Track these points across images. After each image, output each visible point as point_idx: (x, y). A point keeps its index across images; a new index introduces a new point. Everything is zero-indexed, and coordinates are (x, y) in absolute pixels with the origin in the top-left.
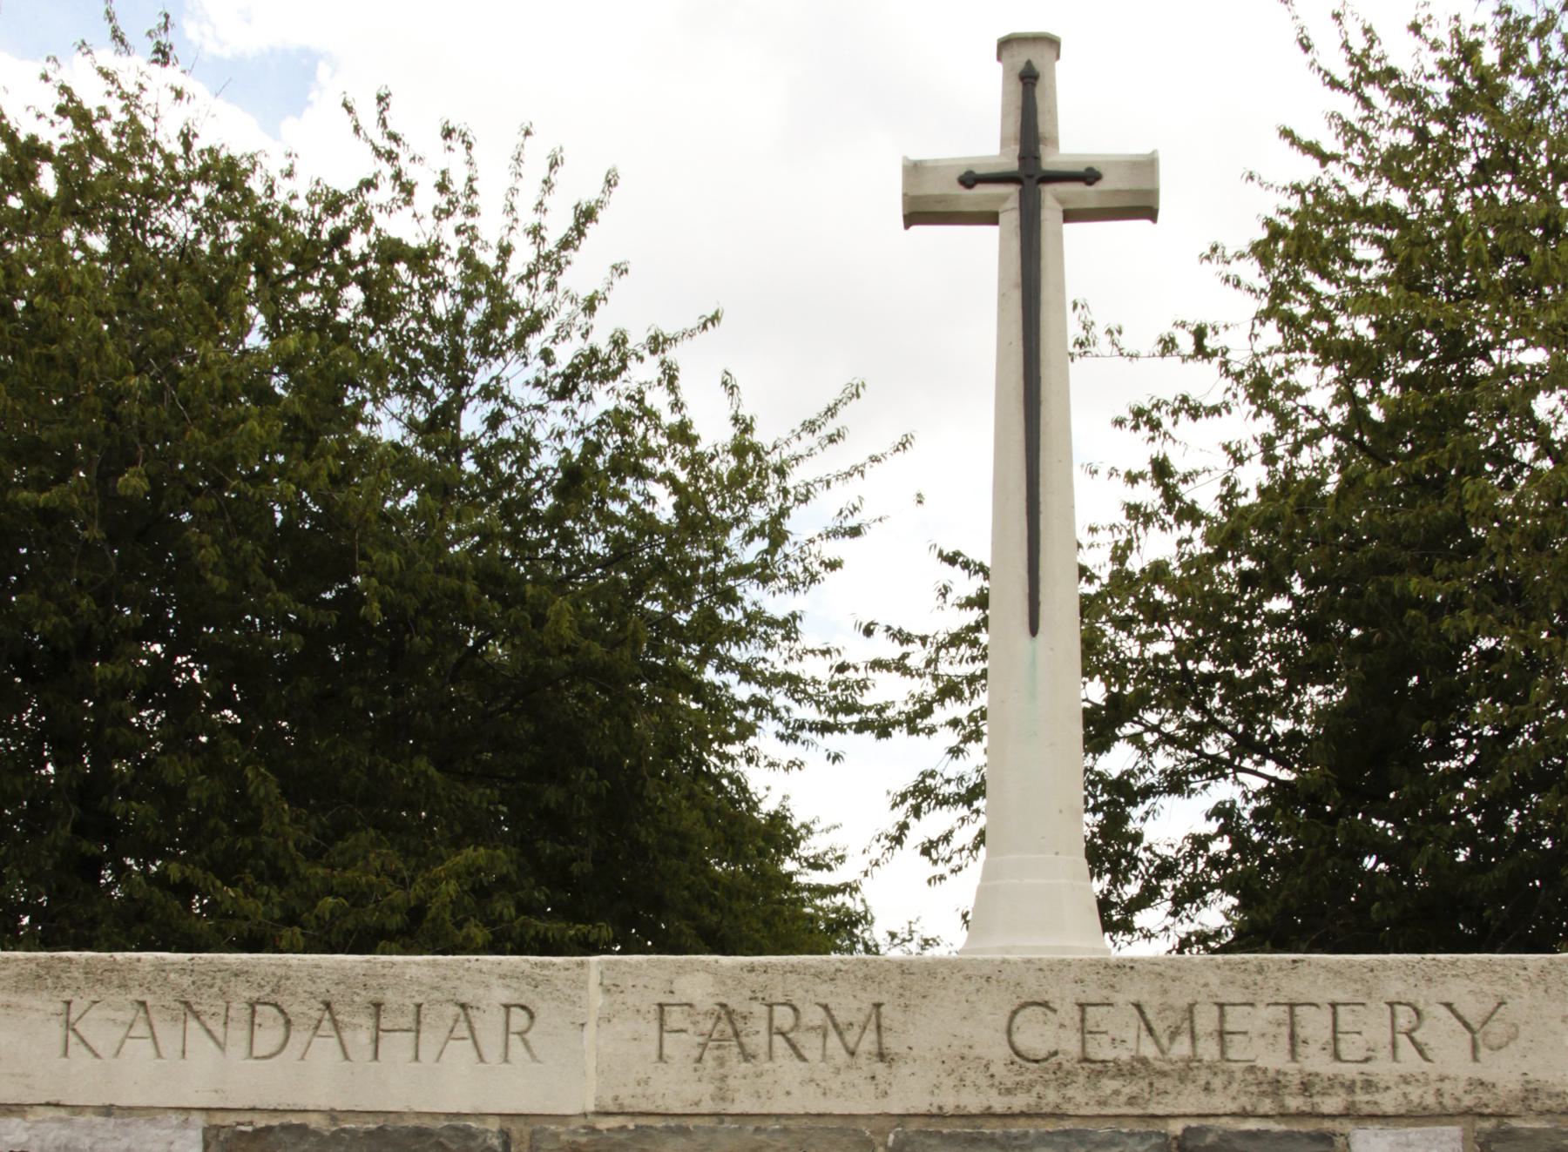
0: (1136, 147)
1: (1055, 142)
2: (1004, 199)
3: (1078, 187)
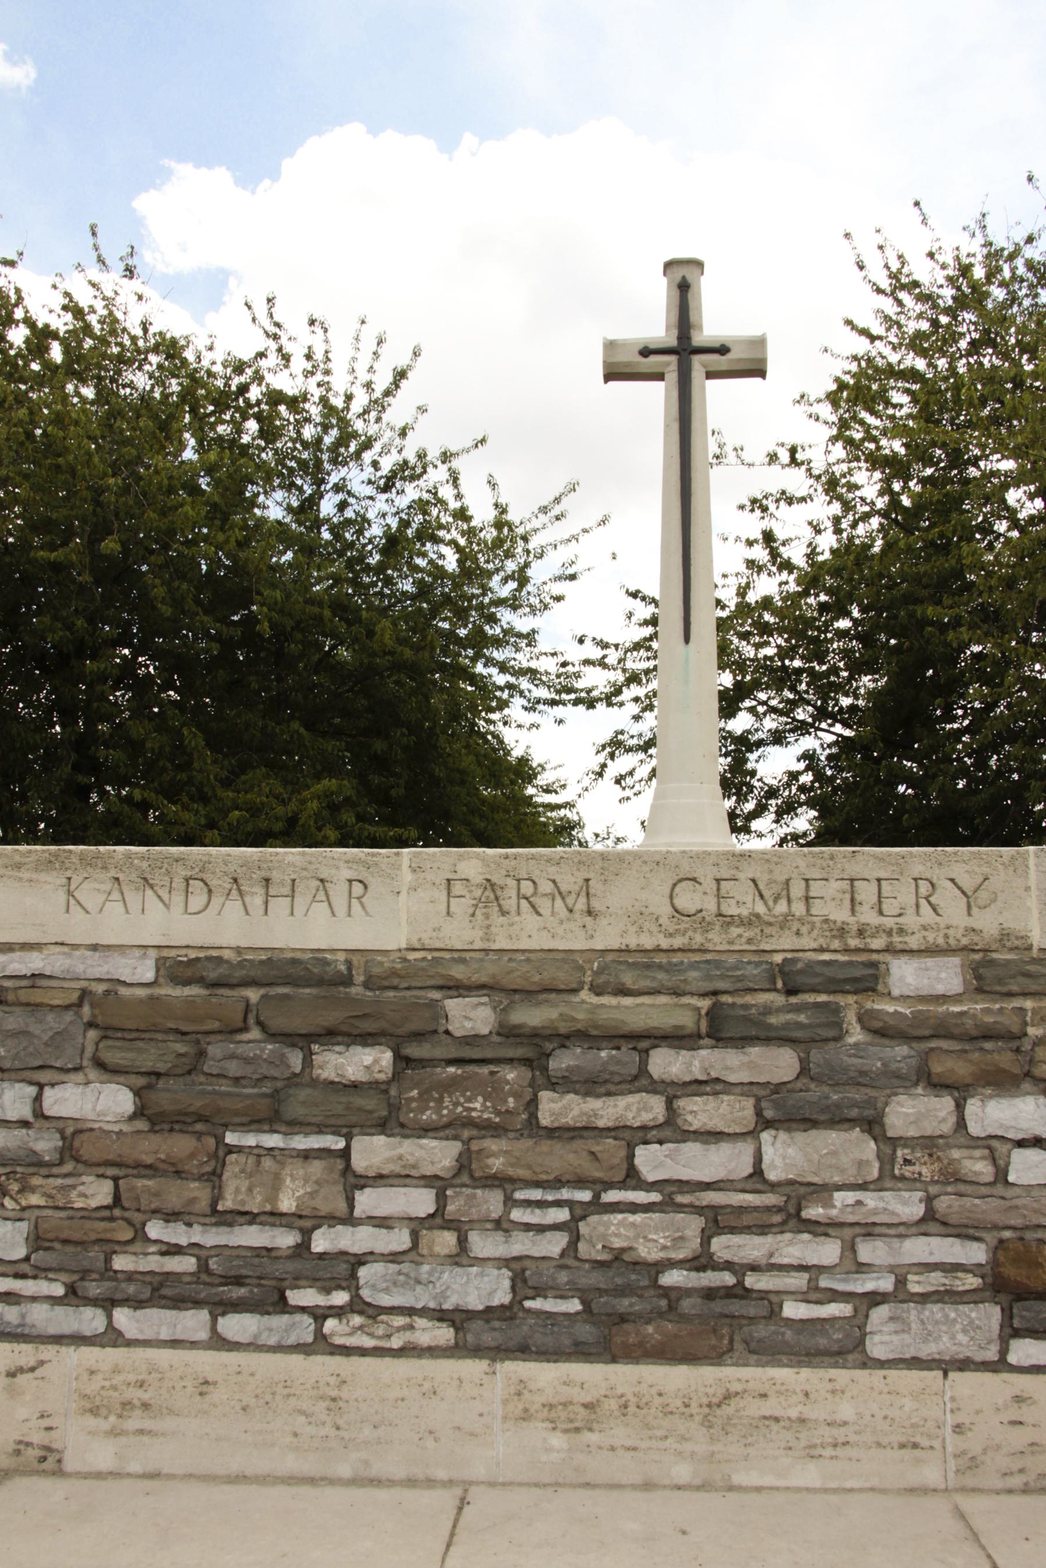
0: (759, 334)
1: (700, 328)
2: (668, 364)
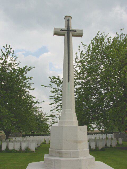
0: (81, 29)
1: (71, 27)
2: (65, 33)
3: (74, 32)
